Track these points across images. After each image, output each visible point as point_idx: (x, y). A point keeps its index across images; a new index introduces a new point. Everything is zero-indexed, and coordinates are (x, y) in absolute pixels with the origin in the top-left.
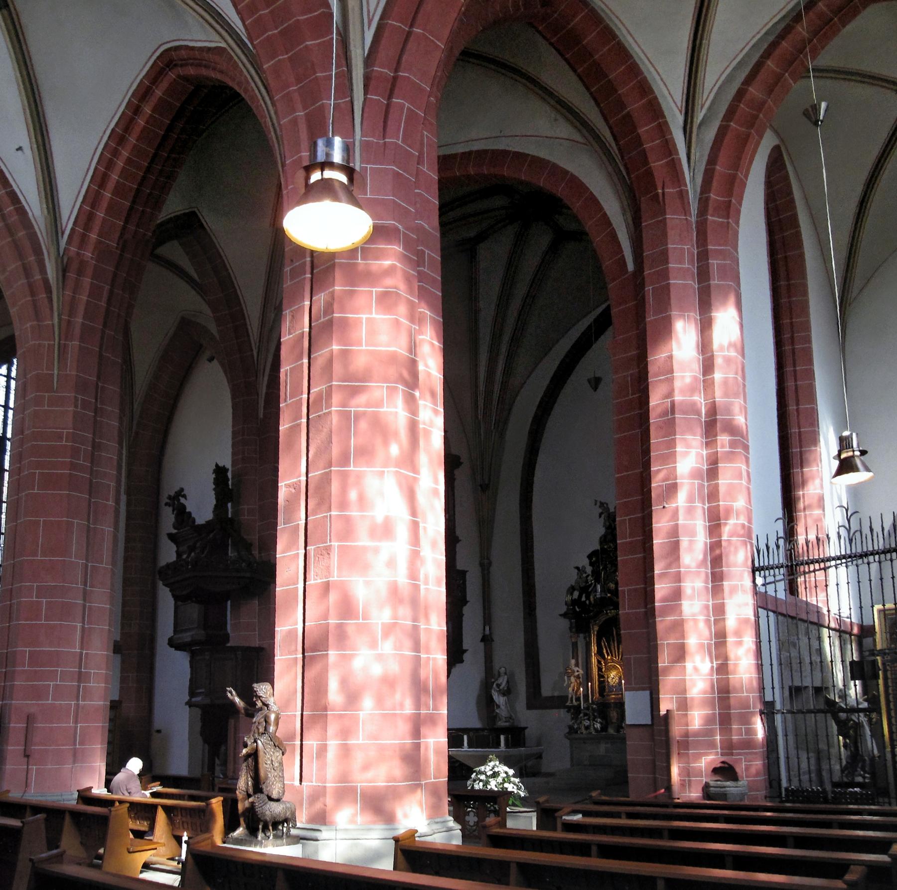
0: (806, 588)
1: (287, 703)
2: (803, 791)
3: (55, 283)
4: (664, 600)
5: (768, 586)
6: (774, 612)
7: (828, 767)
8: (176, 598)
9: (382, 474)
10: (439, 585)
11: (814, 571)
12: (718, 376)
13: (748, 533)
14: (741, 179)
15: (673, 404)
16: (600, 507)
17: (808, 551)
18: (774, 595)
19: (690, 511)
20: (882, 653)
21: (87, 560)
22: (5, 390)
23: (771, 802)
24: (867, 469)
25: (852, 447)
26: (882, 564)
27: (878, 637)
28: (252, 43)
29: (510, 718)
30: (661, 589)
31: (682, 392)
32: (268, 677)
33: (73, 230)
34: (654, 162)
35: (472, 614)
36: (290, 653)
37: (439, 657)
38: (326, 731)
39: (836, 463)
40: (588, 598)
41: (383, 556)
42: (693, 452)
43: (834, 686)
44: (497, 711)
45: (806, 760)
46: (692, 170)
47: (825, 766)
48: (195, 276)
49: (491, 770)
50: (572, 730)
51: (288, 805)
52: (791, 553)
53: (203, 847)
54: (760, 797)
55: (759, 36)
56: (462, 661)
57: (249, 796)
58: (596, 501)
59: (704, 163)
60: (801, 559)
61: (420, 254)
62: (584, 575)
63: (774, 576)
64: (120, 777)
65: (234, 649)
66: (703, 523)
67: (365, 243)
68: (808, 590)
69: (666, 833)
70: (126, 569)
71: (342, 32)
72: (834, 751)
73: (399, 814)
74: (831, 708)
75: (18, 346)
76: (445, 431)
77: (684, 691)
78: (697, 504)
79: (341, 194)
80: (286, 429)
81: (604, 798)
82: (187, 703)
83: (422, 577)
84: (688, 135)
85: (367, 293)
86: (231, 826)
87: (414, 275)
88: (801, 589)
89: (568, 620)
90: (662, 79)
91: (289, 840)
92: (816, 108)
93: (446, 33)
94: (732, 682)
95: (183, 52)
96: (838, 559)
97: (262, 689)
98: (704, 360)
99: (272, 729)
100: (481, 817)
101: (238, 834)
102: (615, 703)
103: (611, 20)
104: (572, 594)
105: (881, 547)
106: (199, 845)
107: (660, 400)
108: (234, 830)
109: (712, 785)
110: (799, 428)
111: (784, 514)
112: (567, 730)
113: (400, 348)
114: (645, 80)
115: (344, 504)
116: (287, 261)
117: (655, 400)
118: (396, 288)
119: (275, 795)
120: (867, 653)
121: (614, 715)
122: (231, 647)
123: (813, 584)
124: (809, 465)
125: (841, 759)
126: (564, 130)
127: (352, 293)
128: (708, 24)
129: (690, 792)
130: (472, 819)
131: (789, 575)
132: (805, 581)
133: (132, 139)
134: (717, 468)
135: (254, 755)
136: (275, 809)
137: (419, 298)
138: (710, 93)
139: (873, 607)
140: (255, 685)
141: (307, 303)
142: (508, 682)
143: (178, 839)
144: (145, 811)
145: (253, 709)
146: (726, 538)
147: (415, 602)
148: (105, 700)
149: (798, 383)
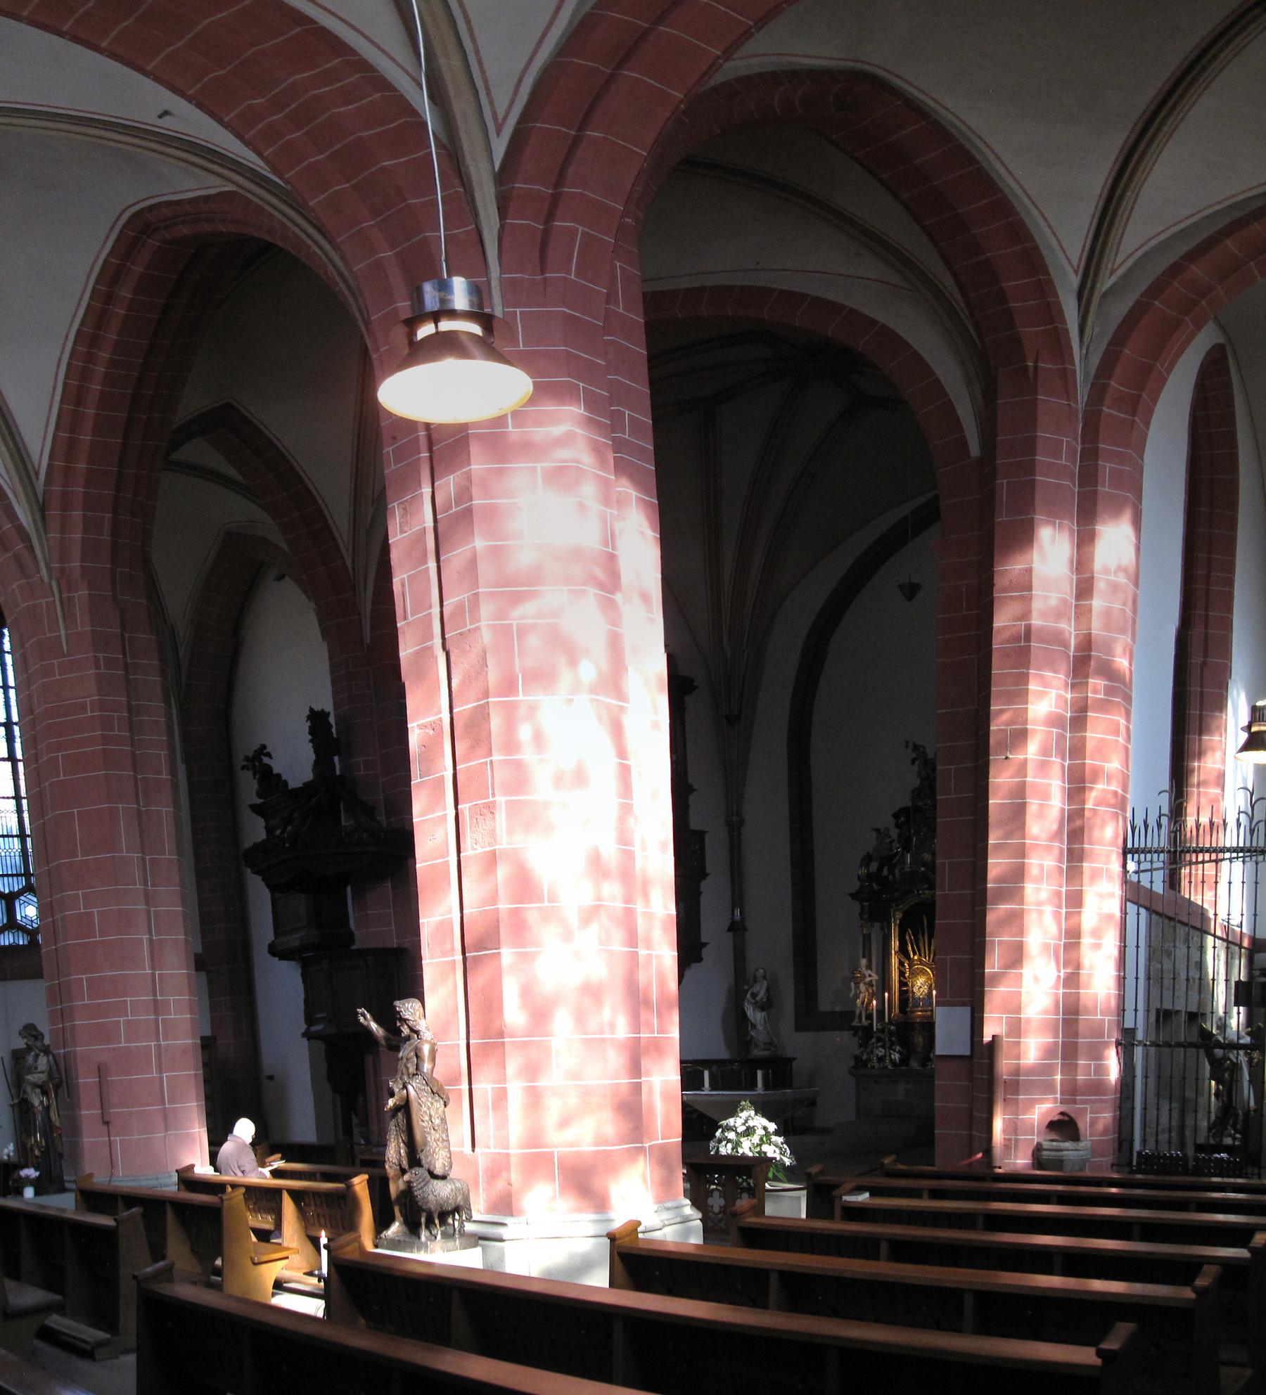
0: (1190, 882)
1: (445, 1028)
2: (1159, 1157)
3: (33, 528)
5: (1141, 874)
6: (1147, 908)
7: (1193, 1122)
11: (1203, 862)
12: (1097, 603)
13: (1121, 803)
15: (1028, 630)
16: (913, 750)
19: (1043, 766)
21: (143, 852)
23: (1118, 1172)
29: (771, 1043)
30: (996, 865)
33: (50, 466)
35: (713, 892)
36: (444, 954)
37: (666, 955)
38: (504, 1068)
39: (1244, 736)
40: (891, 871)
42: (1053, 693)
43: (1212, 1013)
44: (753, 1033)
45: (1167, 1113)
47: (1189, 1122)
48: (238, 477)
49: (744, 1124)
50: (859, 1063)
51: (458, 1185)
53: (350, 1254)
56: (699, 959)
57: (403, 1172)
59: (1106, 342)
62: (888, 840)
63: (1152, 862)
64: (227, 1148)
65: (362, 953)
66: (1060, 783)
67: (522, 407)
68: (1193, 884)
69: (980, 1221)
70: (198, 858)
72: (1202, 1101)
74: (1206, 1041)
77: (1018, 1009)
78: (1054, 759)
79: (473, 348)
81: (901, 1167)
82: (304, 1035)
84: (1082, 307)
86: (382, 1222)
88: (1184, 883)
89: (858, 902)
90: (1050, 227)
91: (464, 1240)
94: (1083, 1000)
97: (408, 1008)
98: (1079, 581)
99: (426, 1066)
100: (730, 1199)
102: (922, 1024)
104: (868, 866)
106: (339, 1252)
107: (1009, 621)
108: (387, 1226)
110: (1202, 687)
111: (1171, 787)
112: (852, 1063)
113: (591, 538)
114: (1022, 223)
115: (511, 745)
117: (1003, 620)
119: (438, 1170)
120: (1258, 973)
121: (919, 1040)
122: (358, 950)
124: (1209, 732)
125: (1209, 1112)
129: (1016, 1157)
130: (716, 1202)
131: (1171, 864)
135: (405, 1107)
136: (441, 1192)
140: (397, 1003)
141: (427, 490)
142: (768, 990)
143: (315, 1241)
144: (265, 1198)
145: (397, 1038)
147: (627, 875)
149: (1205, 690)
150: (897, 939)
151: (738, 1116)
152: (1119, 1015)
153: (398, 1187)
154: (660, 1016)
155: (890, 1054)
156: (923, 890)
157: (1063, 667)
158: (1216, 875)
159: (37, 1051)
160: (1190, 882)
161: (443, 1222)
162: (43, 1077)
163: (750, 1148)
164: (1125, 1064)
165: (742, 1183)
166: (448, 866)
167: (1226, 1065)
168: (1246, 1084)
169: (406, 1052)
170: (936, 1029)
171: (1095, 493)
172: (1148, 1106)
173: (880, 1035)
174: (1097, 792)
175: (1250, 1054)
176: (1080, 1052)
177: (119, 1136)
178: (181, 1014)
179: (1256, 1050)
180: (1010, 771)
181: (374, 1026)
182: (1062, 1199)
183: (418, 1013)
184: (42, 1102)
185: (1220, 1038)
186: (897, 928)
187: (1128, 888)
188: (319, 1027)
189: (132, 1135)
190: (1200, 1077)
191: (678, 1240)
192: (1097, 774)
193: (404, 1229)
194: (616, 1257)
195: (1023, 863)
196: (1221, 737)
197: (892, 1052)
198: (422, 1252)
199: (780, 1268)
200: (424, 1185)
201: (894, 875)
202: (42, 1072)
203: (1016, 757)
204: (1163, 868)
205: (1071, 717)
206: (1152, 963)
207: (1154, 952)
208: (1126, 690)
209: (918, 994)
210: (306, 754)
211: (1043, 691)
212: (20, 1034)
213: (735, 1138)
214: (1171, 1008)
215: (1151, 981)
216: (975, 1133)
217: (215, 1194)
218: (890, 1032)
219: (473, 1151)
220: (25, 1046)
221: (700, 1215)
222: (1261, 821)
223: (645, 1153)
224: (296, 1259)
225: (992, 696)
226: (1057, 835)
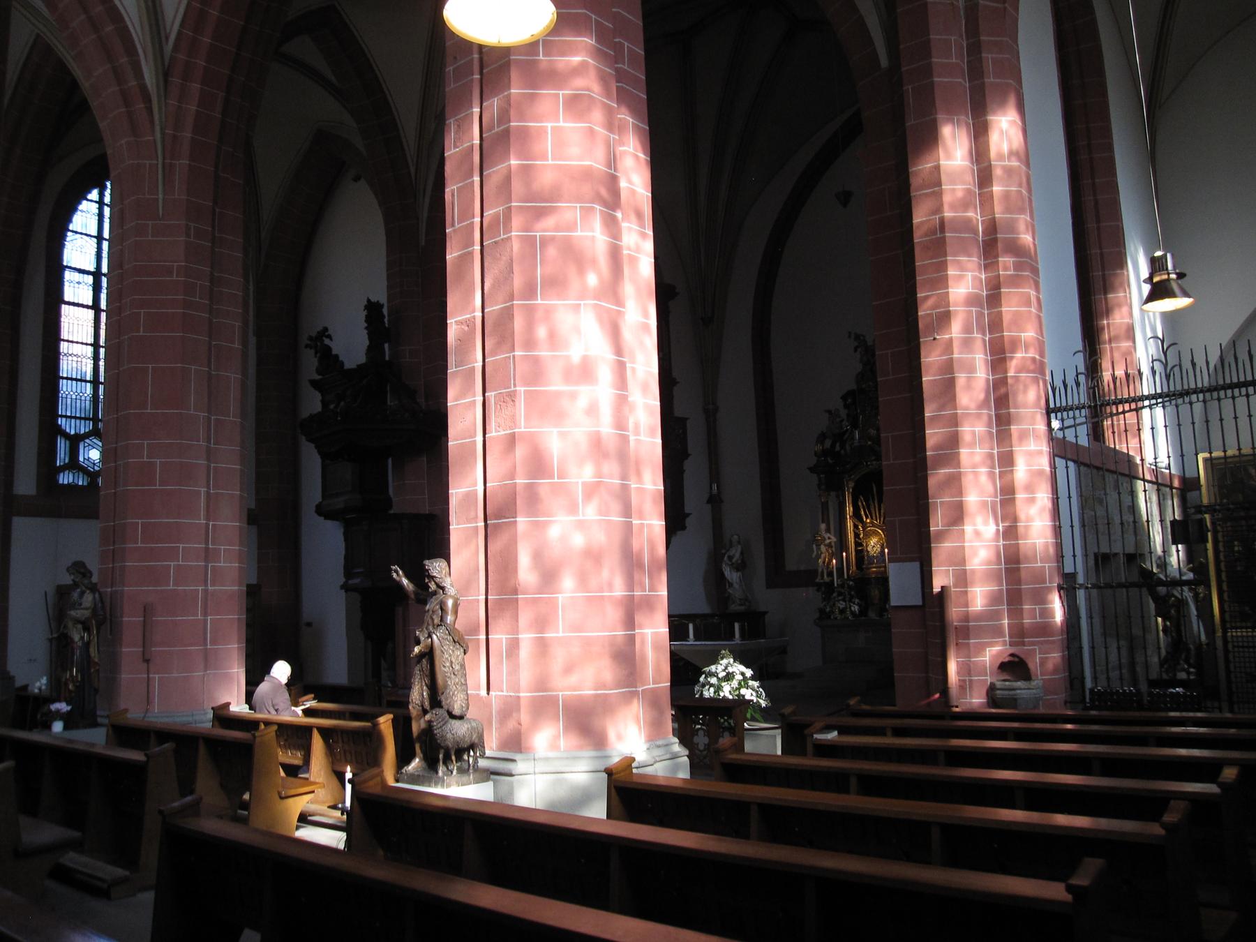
0: (1113, 433)
1: (467, 586)
4: (938, 447)
5: (1066, 430)
8: (324, 456)
9: (577, 308)
10: (652, 435)
12: (997, 189)
13: (1040, 368)
15: (942, 221)
17: (1115, 388)
18: (1075, 441)
19: (967, 343)
20: (1210, 509)
21: (209, 412)
22: (97, 218)
23: (1072, 709)
24: (1186, 294)
25: (1167, 269)
26: (1208, 404)
27: (1204, 490)
30: (933, 435)
31: (953, 207)
32: (443, 552)
33: (180, 33)
35: (694, 469)
37: (654, 524)
38: (517, 621)
39: (1146, 288)
41: (582, 403)
43: (1151, 553)
44: (730, 591)
45: (1116, 651)
47: (1139, 659)
48: (333, 79)
49: (724, 670)
50: (824, 615)
51: (474, 724)
53: (372, 788)
54: (1057, 703)
56: (684, 528)
57: (425, 712)
58: (850, 333)
60: (1107, 398)
61: (618, 48)
62: (838, 420)
63: (1074, 418)
64: (263, 688)
67: (548, 35)
68: (1116, 434)
72: (1150, 638)
73: (612, 735)
75: (111, 166)
76: (656, 258)
77: (963, 562)
80: (455, 257)
82: (342, 587)
83: (631, 426)
85: (551, 99)
86: (403, 758)
87: (610, 73)
88: (1108, 434)
91: (477, 775)
97: (436, 567)
99: (449, 618)
100: (713, 736)
101: (414, 768)
104: (822, 443)
105: (1206, 384)
107: (926, 216)
108: (408, 762)
109: (998, 687)
110: (1101, 248)
111: (1085, 347)
112: (817, 615)
113: (596, 162)
115: (530, 343)
117: (918, 219)
118: (588, 90)
119: (457, 711)
121: (875, 593)
122: (395, 514)
125: (1159, 648)
127: (532, 97)
129: (971, 697)
130: (701, 740)
131: (1093, 418)
132: (1113, 425)
135: (429, 654)
136: (458, 730)
137: (618, 103)
139: (1197, 454)
140: (427, 562)
141: (476, 110)
142: (742, 553)
143: (340, 777)
144: (296, 736)
145: (424, 593)
146: (1013, 374)
147: (623, 456)
148: (240, 585)
149: (1104, 250)
150: (851, 505)
151: (719, 663)
152: (1058, 562)
153: (420, 726)
154: (651, 577)
155: (850, 606)
157: (975, 251)
158: (1138, 422)
159: (84, 588)
160: (1113, 433)
161: (459, 758)
162: (87, 613)
163: (730, 692)
164: (1068, 606)
165: (723, 723)
166: (475, 445)
167: (1171, 602)
168: (1194, 619)
169: (432, 605)
170: (890, 583)
171: (983, 84)
172: (1095, 645)
174: (1019, 357)
175: (1194, 590)
176: (1024, 598)
177: (158, 674)
178: (230, 563)
180: (938, 352)
181: (405, 581)
183: (444, 572)
184: (82, 638)
185: (1162, 577)
186: (850, 495)
187: (1054, 444)
188: (356, 581)
189: (172, 673)
191: (668, 775)
192: (1015, 344)
193: (424, 765)
195: (957, 431)
196: (1126, 292)
197: (852, 604)
198: (439, 786)
200: (444, 725)
202: (86, 609)
204: (1086, 423)
205: (986, 295)
206: (1085, 511)
207: (1086, 502)
208: (1033, 263)
209: (872, 553)
211: (960, 275)
212: (68, 570)
213: (717, 683)
214: (1108, 551)
215: (1086, 528)
216: (931, 675)
217: (248, 731)
218: (849, 587)
219: (488, 694)
220: (71, 582)
221: (687, 752)
223: (639, 696)
224: (321, 793)
225: (918, 285)
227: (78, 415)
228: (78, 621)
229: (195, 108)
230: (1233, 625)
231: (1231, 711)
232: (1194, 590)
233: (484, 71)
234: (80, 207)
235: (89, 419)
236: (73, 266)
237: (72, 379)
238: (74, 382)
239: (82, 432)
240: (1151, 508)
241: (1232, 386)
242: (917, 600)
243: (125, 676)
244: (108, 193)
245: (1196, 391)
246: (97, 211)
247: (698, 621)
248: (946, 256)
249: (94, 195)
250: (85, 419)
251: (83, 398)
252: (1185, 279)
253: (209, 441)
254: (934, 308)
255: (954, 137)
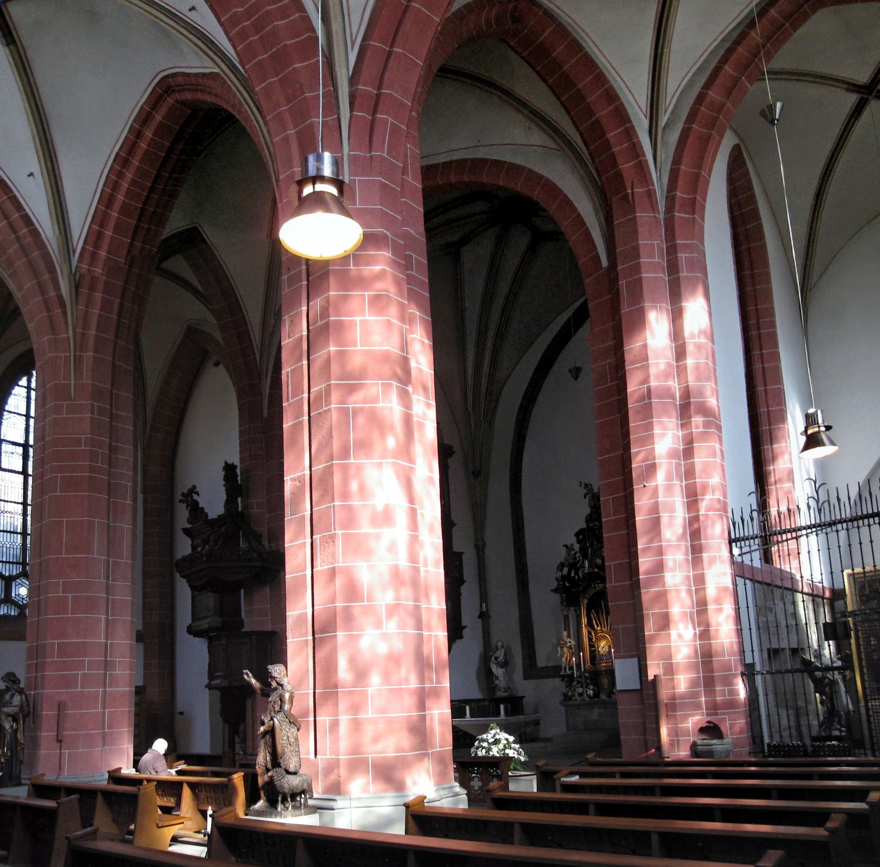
0: (779, 556)
1: (300, 683)
2: (784, 746)
4: (648, 572)
5: (744, 556)
6: (751, 580)
7: (806, 722)
8: (193, 588)
10: (437, 567)
11: (787, 540)
12: (690, 361)
14: (705, 177)
15: (649, 389)
16: (585, 488)
17: (780, 522)
19: (669, 488)
20: (853, 614)
21: (108, 556)
24: (833, 443)
25: (818, 423)
26: (850, 531)
28: (244, 68)
29: (509, 688)
30: (645, 562)
31: (657, 378)
33: (83, 248)
34: (623, 164)
38: (337, 707)
39: (803, 439)
40: (577, 573)
41: (385, 542)
42: (670, 434)
44: (497, 682)
45: (786, 717)
46: (658, 171)
47: (804, 722)
49: (493, 737)
50: (567, 698)
51: (305, 777)
52: (764, 524)
53: (228, 820)
54: (744, 753)
55: (716, 43)
56: (461, 637)
57: (268, 770)
58: (581, 483)
59: (670, 163)
60: (774, 529)
61: (408, 259)
62: (573, 552)
63: (750, 546)
64: (147, 757)
67: (356, 250)
68: (781, 558)
69: (658, 790)
71: (327, 54)
72: (811, 708)
73: (409, 781)
74: (808, 667)
75: (36, 359)
76: (438, 423)
77: (670, 657)
79: (332, 205)
80: (289, 426)
81: (599, 759)
82: (207, 686)
84: (653, 141)
85: (360, 297)
86: (252, 799)
87: (403, 278)
88: (775, 557)
91: (307, 810)
92: (772, 108)
93: (424, 52)
94: (714, 647)
95: (180, 78)
96: (809, 528)
97: (276, 670)
98: (676, 347)
99: (287, 707)
100: (485, 783)
101: (259, 807)
102: (606, 671)
103: (578, 33)
104: (561, 570)
105: (848, 515)
108: (255, 803)
110: (768, 407)
111: (757, 488)
112: (562, 698)
115: (346, 495)
116: (284, 270)
117: (633, 387)
120: (839, 615)
121: (605, 681)
123: (786, 552)
124: (778, 442)
125: (818, 715)
126: (538, 137)
127: (346, 297)
128: (668, 33)
129: (679, 751)
130: (476, 784)
131: (763, 545)
132: (779, 550)
133: (135, 162)
134: (692, 448)
135: (272, 732)
136: (292, 782)
137: (408, 300)
138: (672, 98)
139: (842, 571)
140: (270, 667)
141: (304, 308)
142: (505, 655)
143: (204, 813)
144: (171, 788)
145: (268, 689)
147: (416, 584)
148: (130, 686)
149: (765, 365)
156: (598, 584)
157: (674, 413)
159: (14, 692)
162: (16, 709)
173: (578, 679)
175: (843, 673)
176: (716, 682)
179: (847, 670)
181: (253, 681)
182: (715, 775)
185: (818, 664)
188: (217, 682)
190: (807, 692)
191: (451, 806)
194: (410, 817)
199: (521, 821)
201: (579, 577)
202: (16, 706)
203: (651, 484)
210: (221, 496)
211: (663, 433)
217: (134, 786)
221: (466, 792)
222: (825, 502)
226: (683, 537)
227: (11, 560)
228: (8, 715)
229: (98, 312)
230: (873, 697)
231: (874, 756)
232: (843, 673)
233: (310, 278)
234: (14, 392)
235: (19, 563)
236: (8, 439)
237: (7, 532)
238: (9, 534)
239: (14, 574)
240: (808, 613)
241: (868, 516)
242: (637, 686)
243: (43, 752)
244: (34, 380)
245: (840, 522)
246: (26, 394)
247: (473, 704)
248: (652, 418)
249: (24, 381)
250: (17, 563)
251: (15, 547)
252: (831, 431)
253: (108, 579)
254: (645, 460)
255: (657, 321)
